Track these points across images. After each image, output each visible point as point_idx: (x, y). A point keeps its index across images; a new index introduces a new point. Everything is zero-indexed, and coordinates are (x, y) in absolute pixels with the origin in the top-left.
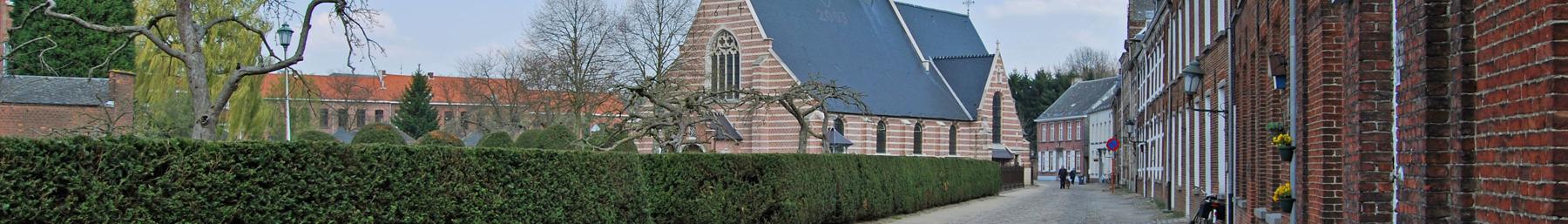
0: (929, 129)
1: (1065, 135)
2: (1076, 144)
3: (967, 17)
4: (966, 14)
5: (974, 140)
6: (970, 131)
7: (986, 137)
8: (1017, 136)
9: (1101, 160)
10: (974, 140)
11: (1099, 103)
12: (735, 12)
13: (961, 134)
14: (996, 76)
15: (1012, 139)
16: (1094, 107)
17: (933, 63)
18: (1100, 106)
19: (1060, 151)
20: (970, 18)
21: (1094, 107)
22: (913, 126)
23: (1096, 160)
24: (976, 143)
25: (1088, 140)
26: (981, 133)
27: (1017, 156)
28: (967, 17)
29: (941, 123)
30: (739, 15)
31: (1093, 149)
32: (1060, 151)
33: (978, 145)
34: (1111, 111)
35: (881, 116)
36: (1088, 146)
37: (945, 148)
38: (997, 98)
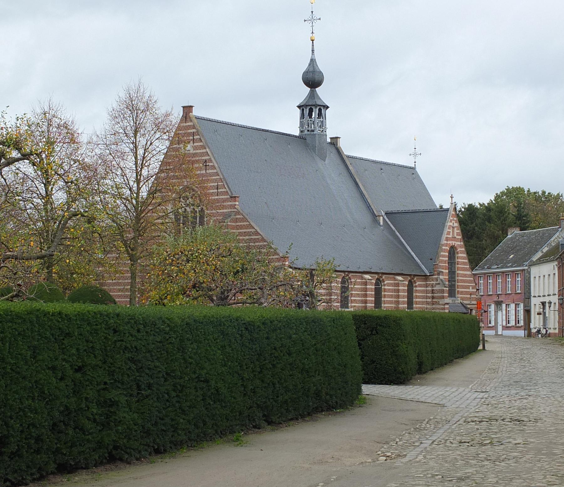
0: (389, 285)
1: (505, 288)
2: (516, 297)
3: (414, 169)
4: (413, 166)
5: (430, 295)
6: (427, 286)
7: (443, 291)
8: (471, 290)
9: (545, 313)
10: (430, 295)
11: (539, 255)
12: (201, 169)
13: (418, 289)
14: (451, 230)
15: (466, 293)
16: (535, 258)
17: (385, 217)
18: (541, 258)
19: (498, 304)
20: (418, 170)
21: (535, 258)
22: (374, 281)
23: (539, 314)
24: (433, 298)
25: (530, 293)
26: (437, 288)
27: (471, 310)
28: (414, 169)
29: (400, 278)
30: (204, 172)
31: (535, 302)
32: (498, 304)
33: (434, 300)
34: (556, 263)
35: (410, 275)
36: (529, 298)
37: (403, 303)
38: (452, 251)
